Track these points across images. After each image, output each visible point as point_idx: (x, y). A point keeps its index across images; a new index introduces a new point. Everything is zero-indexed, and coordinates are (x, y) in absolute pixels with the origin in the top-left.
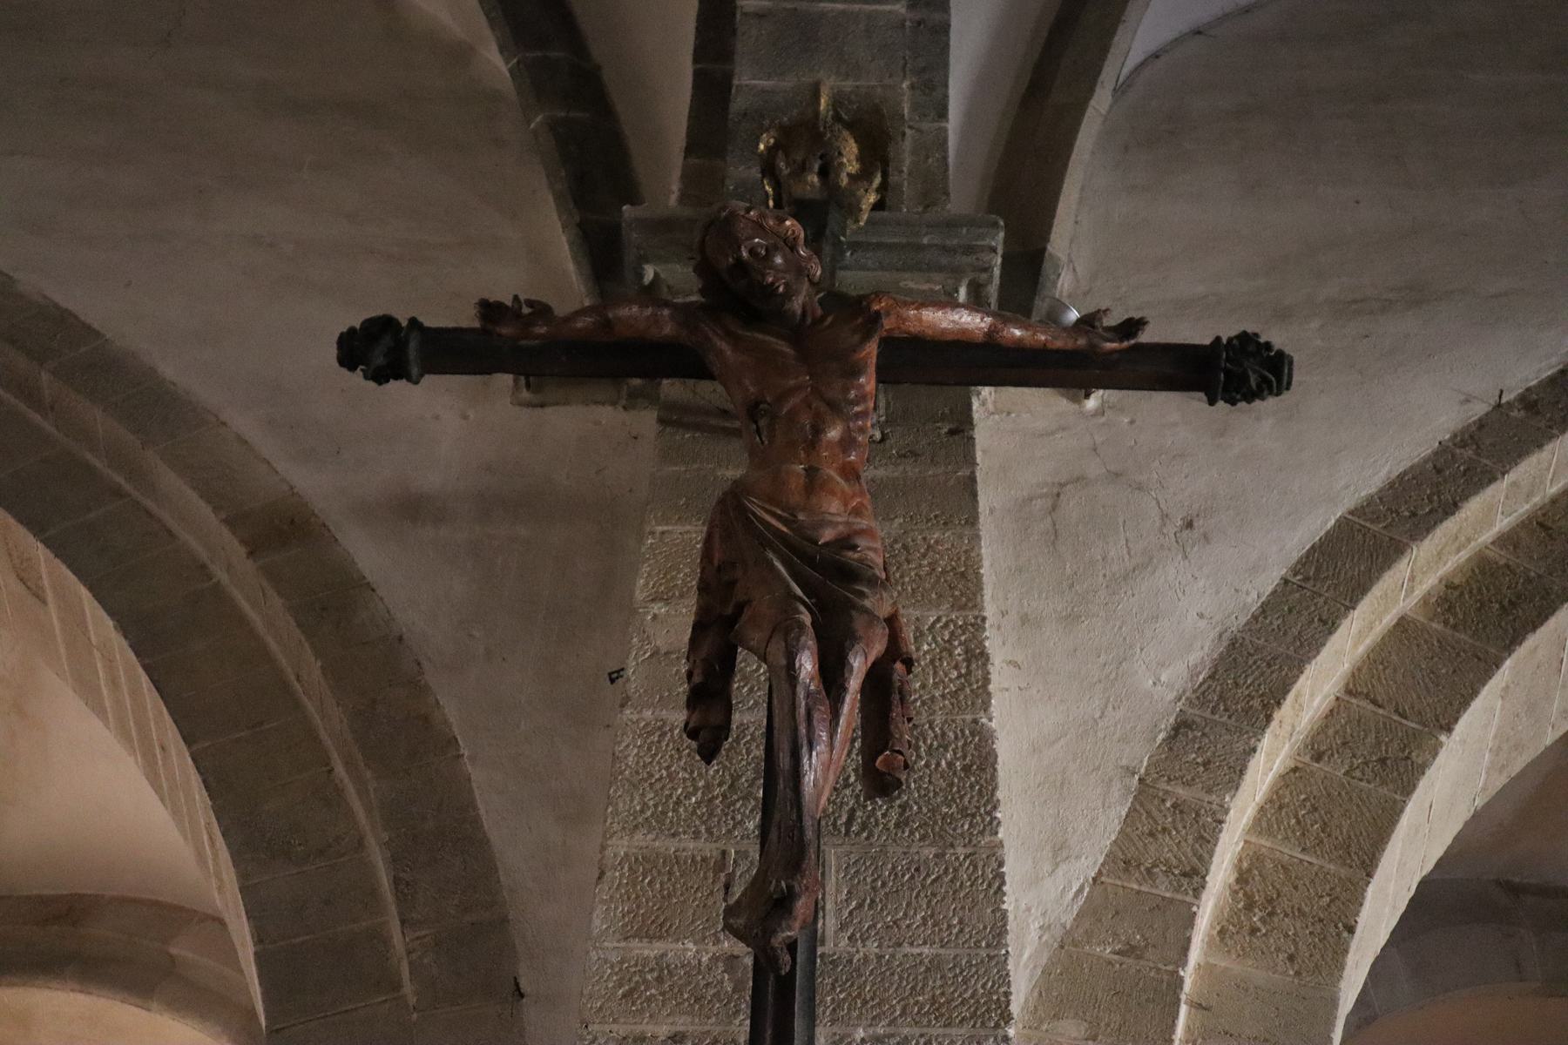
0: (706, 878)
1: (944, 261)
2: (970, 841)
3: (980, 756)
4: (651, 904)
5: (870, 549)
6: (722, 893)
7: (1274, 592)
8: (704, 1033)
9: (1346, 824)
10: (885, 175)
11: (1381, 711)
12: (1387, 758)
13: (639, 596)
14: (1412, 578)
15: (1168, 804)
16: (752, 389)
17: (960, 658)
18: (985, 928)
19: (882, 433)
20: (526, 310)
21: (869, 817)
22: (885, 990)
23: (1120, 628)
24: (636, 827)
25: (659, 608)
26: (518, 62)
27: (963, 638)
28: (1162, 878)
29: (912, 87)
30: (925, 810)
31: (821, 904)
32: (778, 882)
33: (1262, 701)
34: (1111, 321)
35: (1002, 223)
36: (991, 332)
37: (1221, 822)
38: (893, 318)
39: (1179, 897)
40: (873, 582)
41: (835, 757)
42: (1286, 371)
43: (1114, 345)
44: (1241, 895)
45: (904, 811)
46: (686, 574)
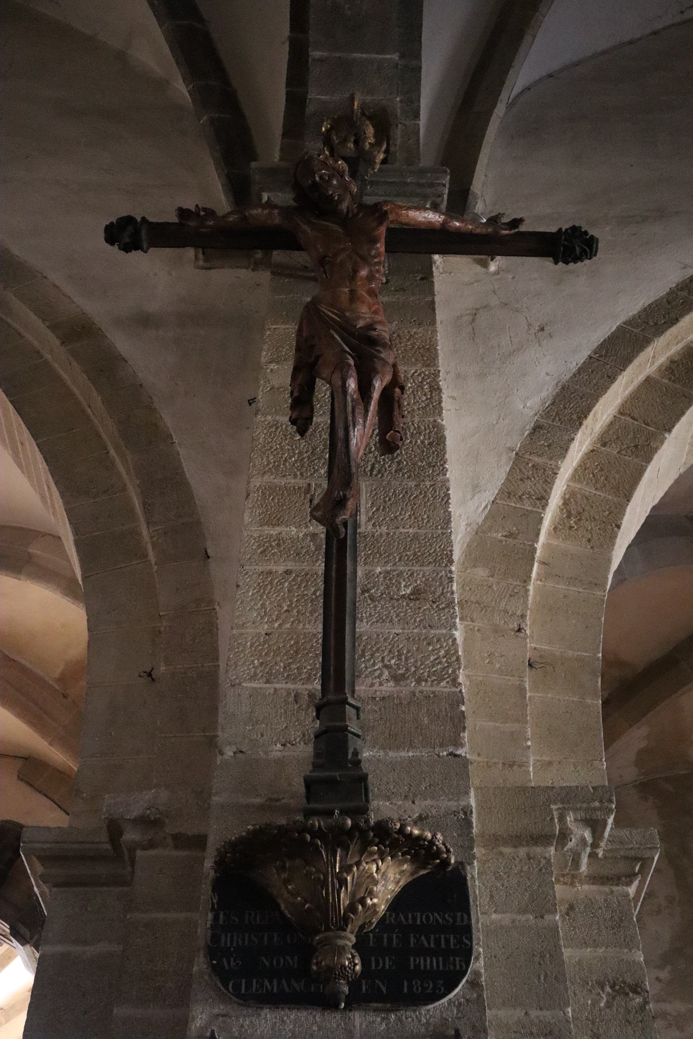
0: (300, 496)
1: (418, 191)
2: (432, 479)
3: (437, 438)
4: (273, 509)
5: (382, 330)
6: (309, 504)
7: (585, 362)
8: (300, 570)
9: (617, 476)
10: (388, 144)
11: (636, 423)
12: (638, 445)
13: (263, 360)
14: (654, 357)
15: (530, 465)
16: (321, 250)
17: (427, 390)
18: (440, 520)
19: (387, 279)
20: (202, 213)
21: (381, 468)
22: (391, 550)
23: (507, 380)
24: (265, 473)
25: (274, 366)
26: (193, 87)
27: (428, 381)
28: (526, 500)
29: (401, 101)
30: (410, 464)
31: (359, 508)
32: (339, 492)
33: (578, 416)
34: (505, 220)
35: (449, 171)
36: (444, 224)
37: (556, 474)
38: (394, 215)
39: (535, 510)
40: (384, 345)
41: (366, 432)
42: (595, 246)
43: (507, 232)
44: (565, 511)
45: (399, 465)
46: (287, 349)
